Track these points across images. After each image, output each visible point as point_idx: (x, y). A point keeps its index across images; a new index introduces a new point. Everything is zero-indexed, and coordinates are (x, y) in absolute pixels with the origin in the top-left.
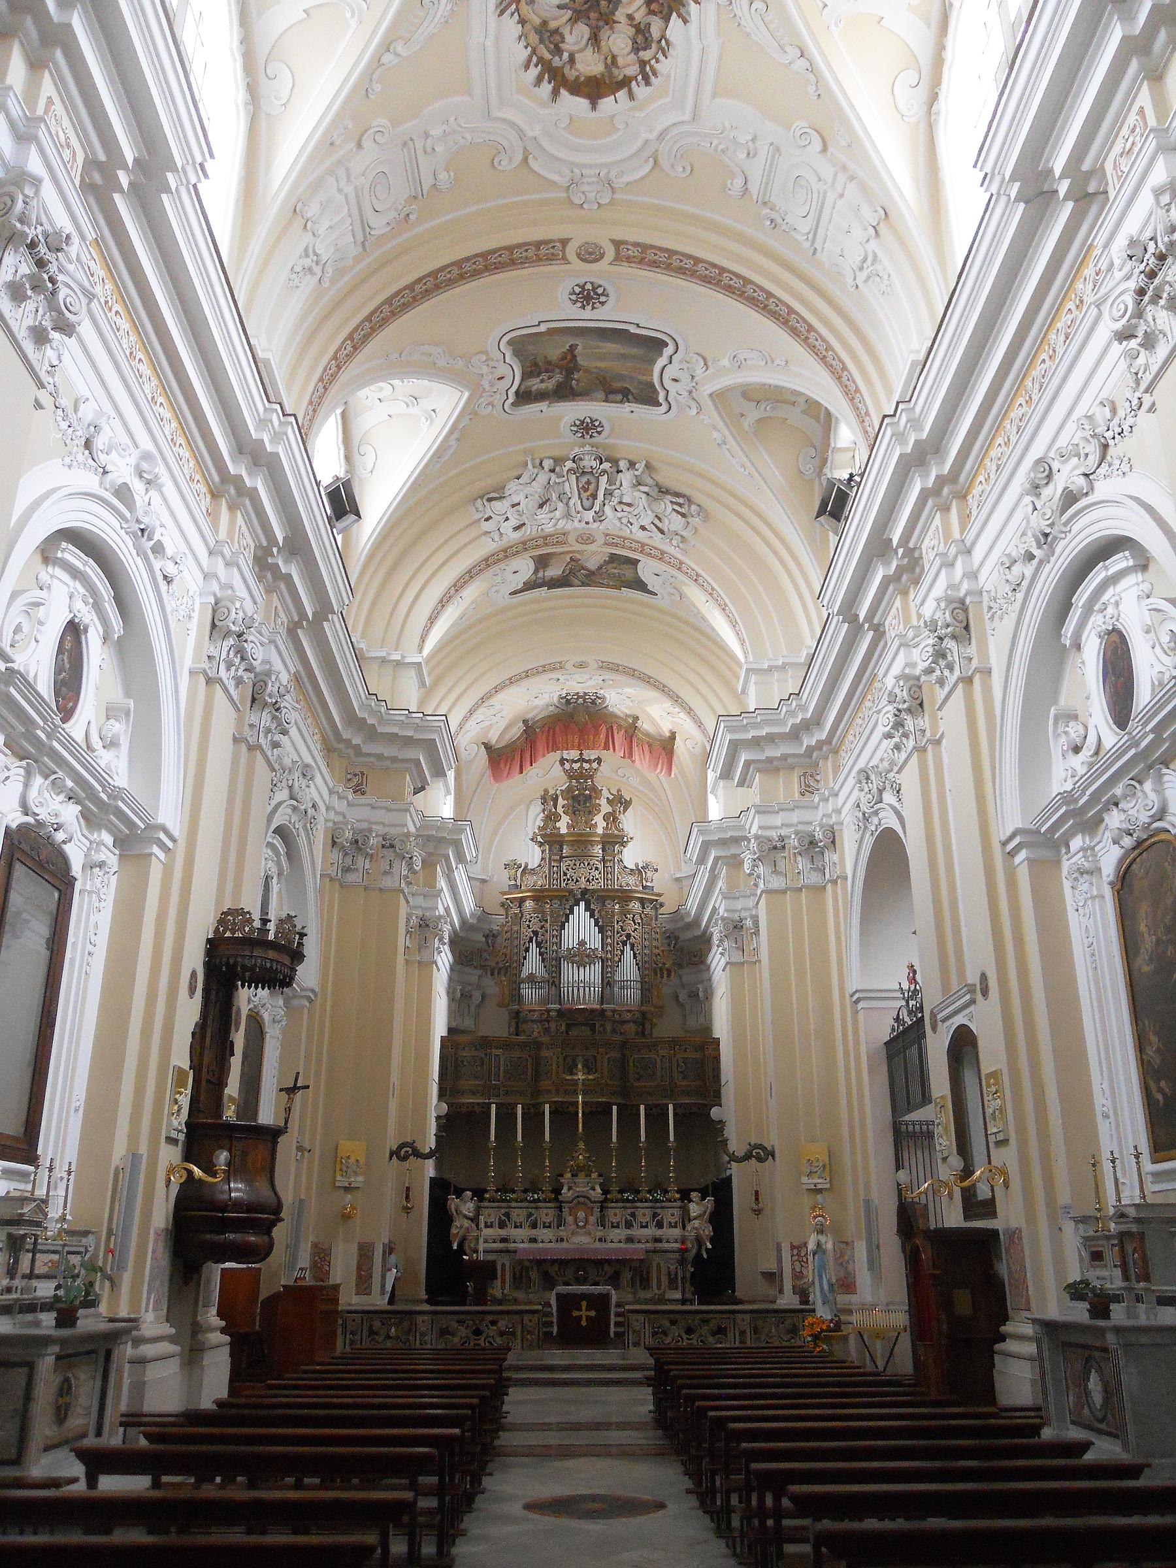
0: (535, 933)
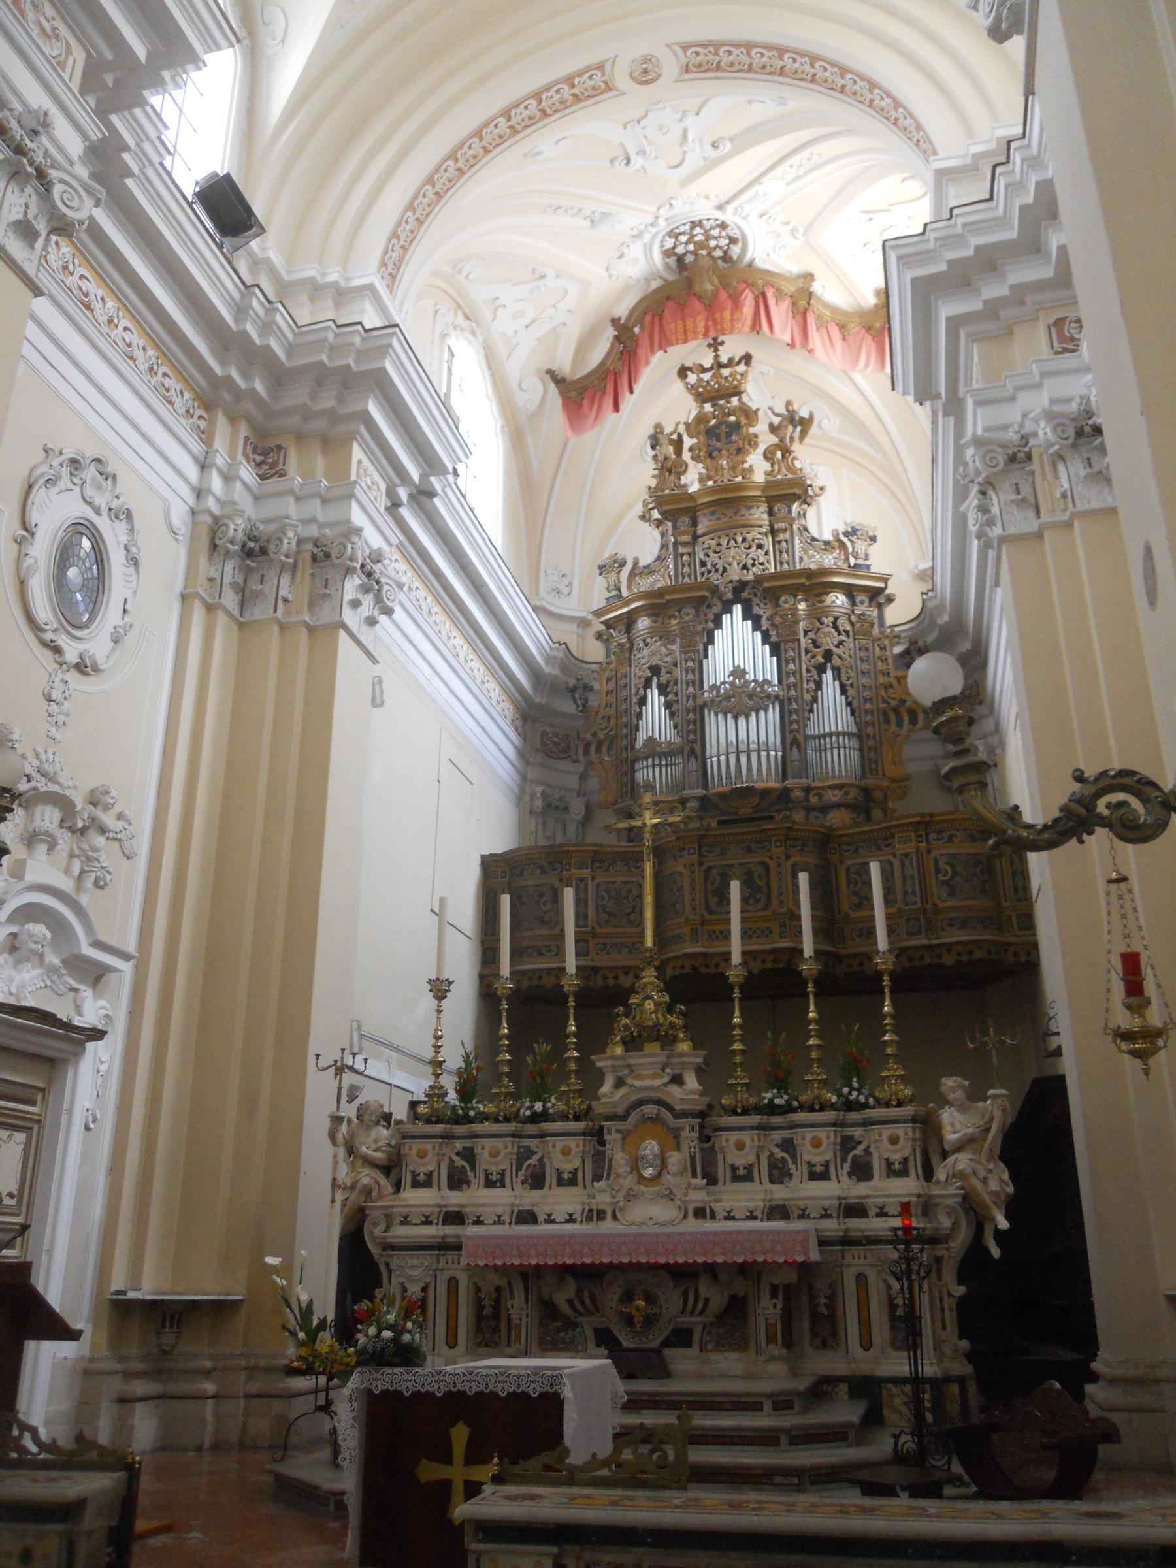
0: (655, 670)
